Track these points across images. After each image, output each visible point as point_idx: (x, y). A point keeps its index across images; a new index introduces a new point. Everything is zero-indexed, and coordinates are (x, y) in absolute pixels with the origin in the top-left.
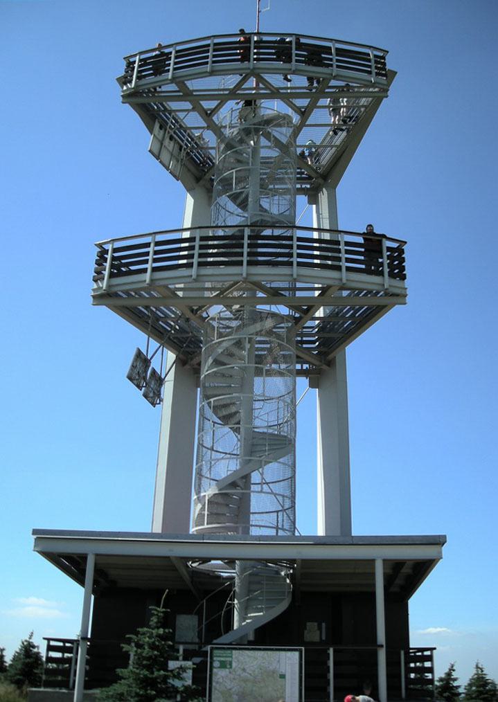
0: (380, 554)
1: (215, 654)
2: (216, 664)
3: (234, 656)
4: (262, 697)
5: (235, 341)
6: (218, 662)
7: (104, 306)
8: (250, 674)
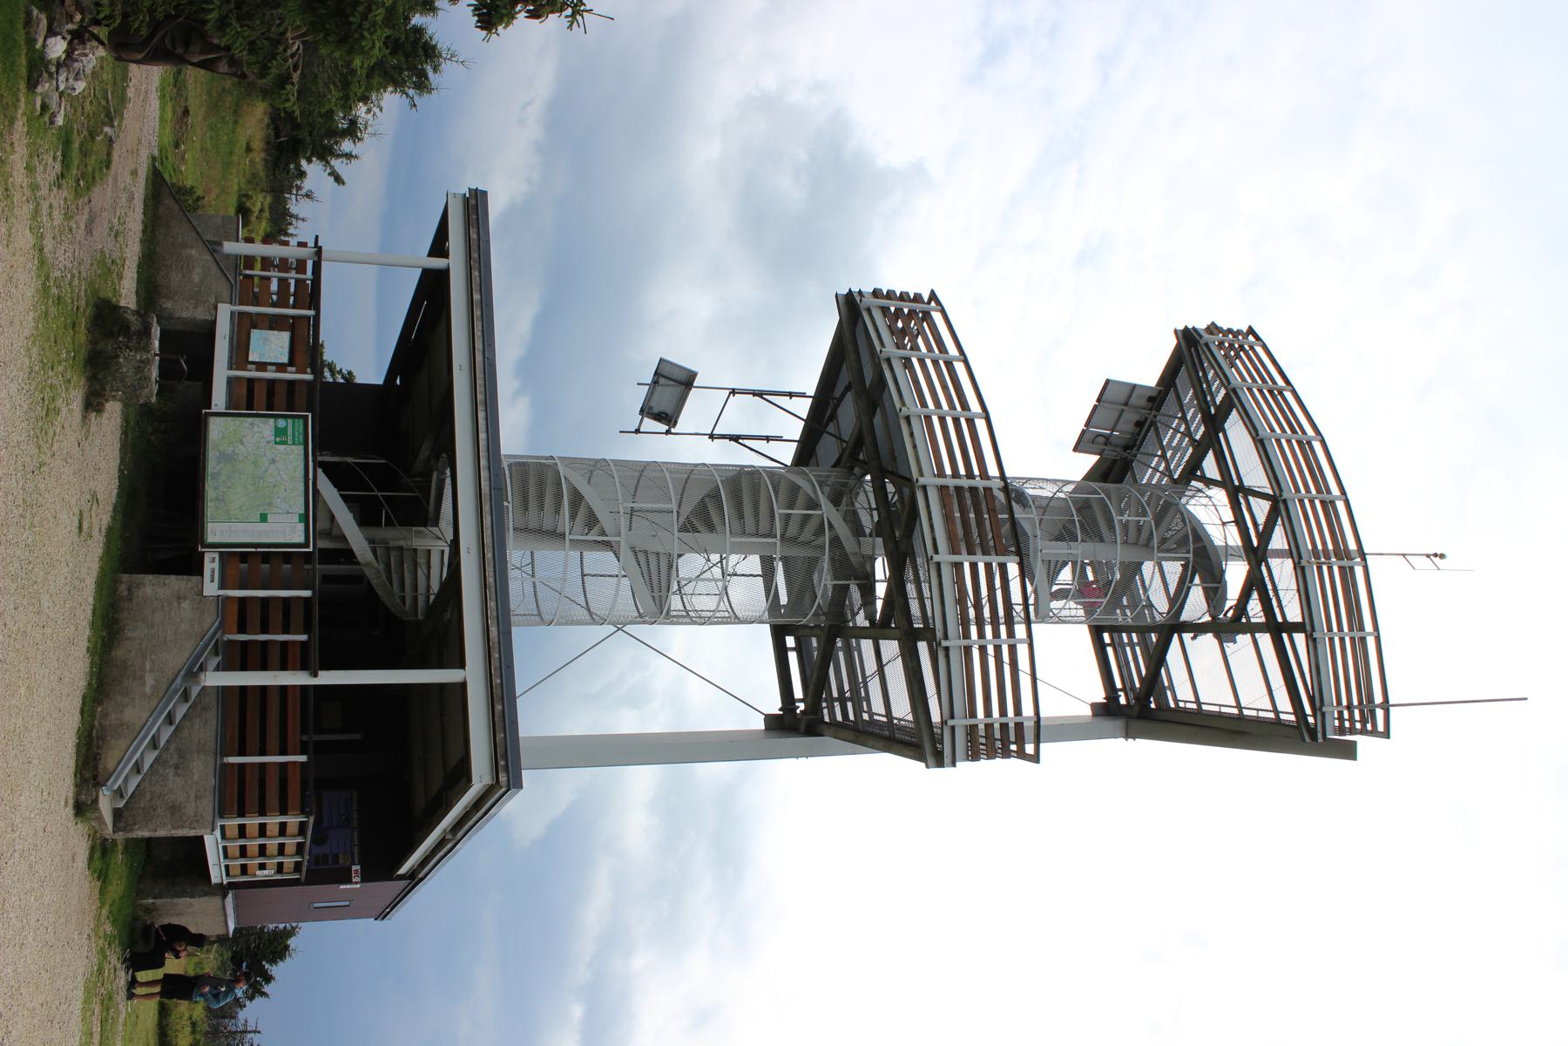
0: (473, 675)
1: (296, 420)
2: (281, 423)
3: (294, 447)
4: (229, 488)
5: (812, 495)
6: (285, 425)
8: (266, 471)
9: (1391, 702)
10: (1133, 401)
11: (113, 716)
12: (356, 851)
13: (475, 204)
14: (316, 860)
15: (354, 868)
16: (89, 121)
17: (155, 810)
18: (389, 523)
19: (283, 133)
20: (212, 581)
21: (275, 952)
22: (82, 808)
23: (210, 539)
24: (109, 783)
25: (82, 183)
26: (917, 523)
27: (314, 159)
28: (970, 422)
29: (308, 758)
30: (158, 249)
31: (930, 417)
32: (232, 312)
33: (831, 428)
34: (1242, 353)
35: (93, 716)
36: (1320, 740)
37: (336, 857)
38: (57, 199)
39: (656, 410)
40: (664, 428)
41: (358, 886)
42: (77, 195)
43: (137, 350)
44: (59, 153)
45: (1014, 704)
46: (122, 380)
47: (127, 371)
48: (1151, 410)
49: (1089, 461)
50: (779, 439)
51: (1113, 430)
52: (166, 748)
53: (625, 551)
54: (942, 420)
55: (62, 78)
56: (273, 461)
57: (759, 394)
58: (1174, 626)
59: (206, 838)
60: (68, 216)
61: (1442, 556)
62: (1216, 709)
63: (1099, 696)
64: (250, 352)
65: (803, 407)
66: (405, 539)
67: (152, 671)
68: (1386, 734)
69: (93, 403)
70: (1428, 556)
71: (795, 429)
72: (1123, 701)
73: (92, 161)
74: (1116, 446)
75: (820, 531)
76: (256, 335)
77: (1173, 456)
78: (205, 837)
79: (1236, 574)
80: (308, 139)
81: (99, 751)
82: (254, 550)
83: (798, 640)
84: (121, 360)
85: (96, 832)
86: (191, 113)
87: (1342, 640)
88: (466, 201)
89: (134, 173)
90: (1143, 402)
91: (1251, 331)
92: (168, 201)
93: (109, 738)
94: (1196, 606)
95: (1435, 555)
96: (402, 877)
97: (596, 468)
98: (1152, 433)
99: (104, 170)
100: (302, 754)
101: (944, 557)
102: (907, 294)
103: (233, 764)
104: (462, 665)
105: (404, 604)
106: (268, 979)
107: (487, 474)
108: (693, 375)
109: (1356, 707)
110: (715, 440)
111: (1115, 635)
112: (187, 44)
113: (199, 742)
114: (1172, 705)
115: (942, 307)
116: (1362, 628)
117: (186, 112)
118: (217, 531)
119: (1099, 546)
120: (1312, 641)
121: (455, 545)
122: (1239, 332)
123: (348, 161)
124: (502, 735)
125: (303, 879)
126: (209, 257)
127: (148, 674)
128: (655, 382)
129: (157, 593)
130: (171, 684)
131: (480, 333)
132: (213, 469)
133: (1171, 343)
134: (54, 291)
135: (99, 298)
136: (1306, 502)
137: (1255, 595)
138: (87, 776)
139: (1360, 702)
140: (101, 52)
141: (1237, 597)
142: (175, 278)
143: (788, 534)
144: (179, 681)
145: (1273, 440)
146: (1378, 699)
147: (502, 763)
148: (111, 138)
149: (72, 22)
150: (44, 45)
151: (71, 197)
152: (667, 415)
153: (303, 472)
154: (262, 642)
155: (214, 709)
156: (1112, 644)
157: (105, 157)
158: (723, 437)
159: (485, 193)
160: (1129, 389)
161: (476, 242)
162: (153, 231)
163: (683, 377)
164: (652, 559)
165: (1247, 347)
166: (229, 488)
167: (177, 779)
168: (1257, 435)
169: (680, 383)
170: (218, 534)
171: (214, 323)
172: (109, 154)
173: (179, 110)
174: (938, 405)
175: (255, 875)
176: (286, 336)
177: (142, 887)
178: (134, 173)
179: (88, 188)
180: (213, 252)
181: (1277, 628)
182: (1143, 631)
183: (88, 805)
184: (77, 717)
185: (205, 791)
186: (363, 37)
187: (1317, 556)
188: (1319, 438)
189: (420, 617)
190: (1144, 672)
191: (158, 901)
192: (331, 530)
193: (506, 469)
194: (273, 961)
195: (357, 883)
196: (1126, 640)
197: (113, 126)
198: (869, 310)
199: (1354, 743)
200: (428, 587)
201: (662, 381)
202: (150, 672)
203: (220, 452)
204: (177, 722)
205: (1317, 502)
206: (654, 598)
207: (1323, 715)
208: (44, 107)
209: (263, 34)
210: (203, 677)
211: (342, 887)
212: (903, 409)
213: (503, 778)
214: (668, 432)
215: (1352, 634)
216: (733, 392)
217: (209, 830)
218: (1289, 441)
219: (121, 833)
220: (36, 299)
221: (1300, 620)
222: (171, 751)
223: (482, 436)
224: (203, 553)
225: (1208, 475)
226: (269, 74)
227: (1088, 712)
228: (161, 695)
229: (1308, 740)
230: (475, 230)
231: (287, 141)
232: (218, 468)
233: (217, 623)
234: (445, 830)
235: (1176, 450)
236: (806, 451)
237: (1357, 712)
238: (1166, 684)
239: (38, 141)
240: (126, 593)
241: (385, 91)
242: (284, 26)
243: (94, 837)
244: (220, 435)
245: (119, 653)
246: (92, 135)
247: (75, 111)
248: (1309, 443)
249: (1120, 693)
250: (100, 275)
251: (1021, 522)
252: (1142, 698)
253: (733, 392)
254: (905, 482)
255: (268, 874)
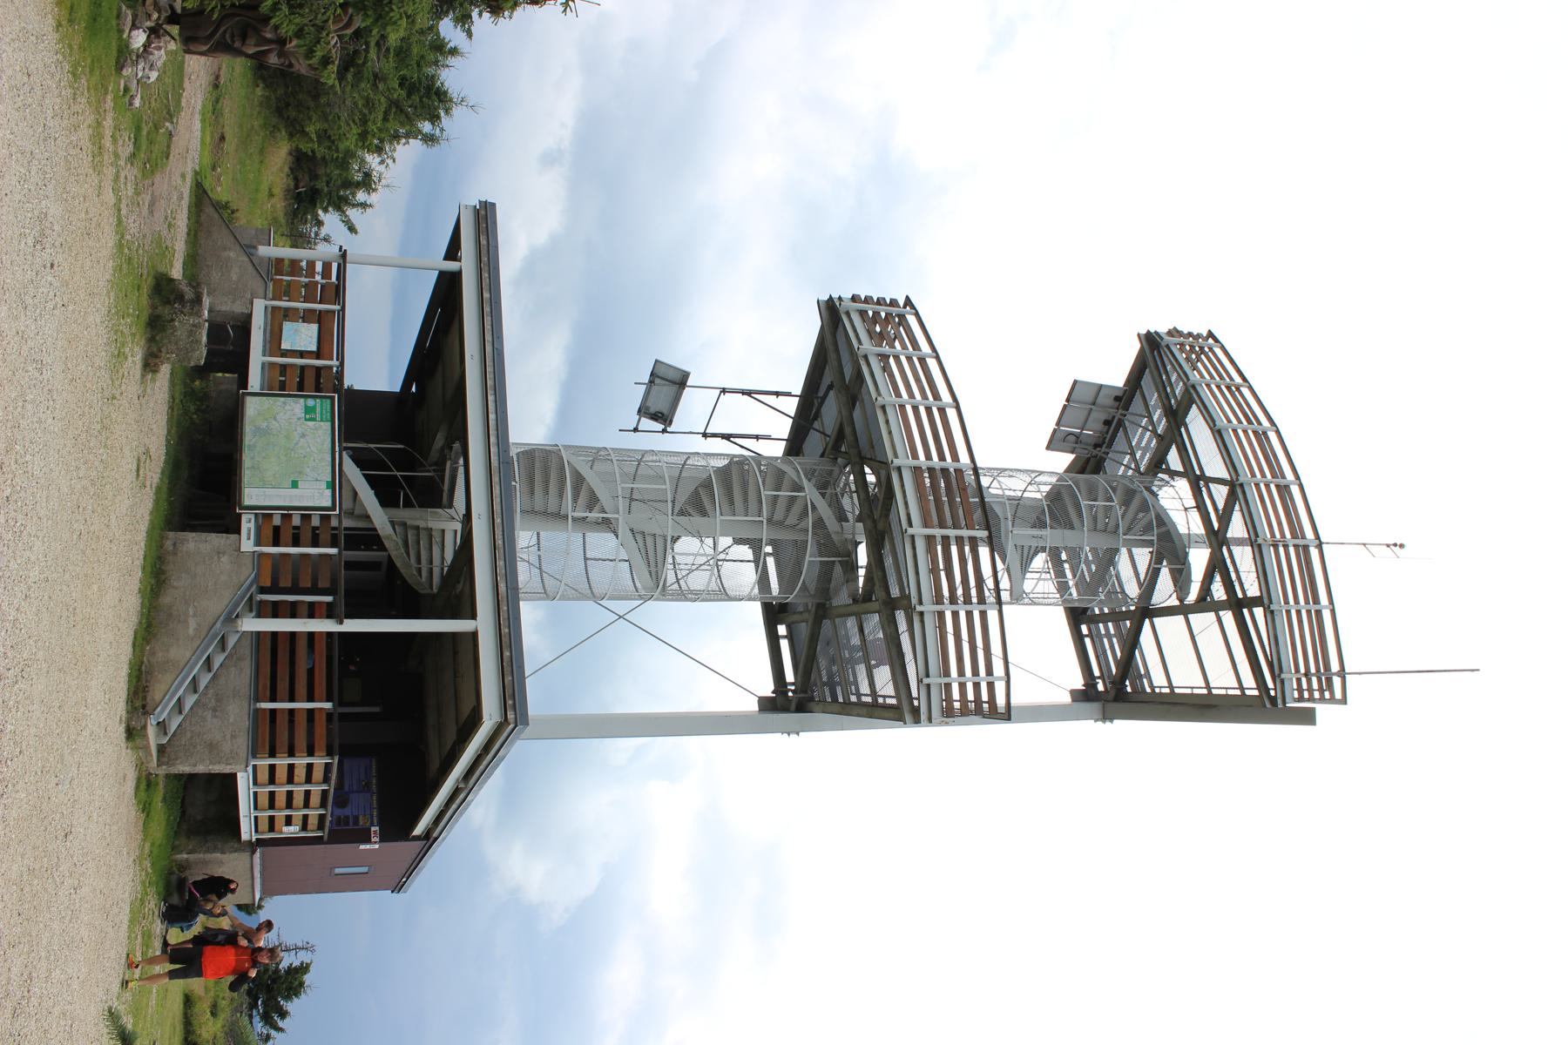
0: (483, 624)
1: (324, 400)
2: (311, 402)
3: (322, 423)
4: (264, 458)
5: (796, 480)
7: (820, 324)
8: (297, 444)
9: (1347, 671)
10: (1099, 401)
11: (160, 654)
12: (375, 813)
13: (485, 216)
14: (338, 821)
15: (373, 829)
16: (154, 115)
17: (195, 747)
18: (408, 504)
19: (301, 184)
20: (249, 539)
21: (291, 988)
22: (133, 734)
23: (247, 502)
24: (156, 712)
25: (148, 166)
26: (894, 503)
27: (330, 209)
28: (942, 411)
29: (334, 706)
30: (200, 251)
31: (904, 406)
32: (266, 307)
33: (816, 425)
34: (1203, 356)
35: (142, 651)
36: (1280, 706)
37: (356, 819)
38: (130, 173)
39: (652, 410)
40: (660, 427)
41: (377, 846)
42: (144, 176)
43: (191, 314)
44: (132, 136)
45: (986, 665)
46: (176, 344)
47: (181, 335)
48: (1118, 409)
49: (1062, 460)
50: (768, 438)
51: (1082, 430)
52: (205, 693)
53: (623, 529)
54: (915, 409)
55: (140, 67)
56: (303, 436)
57: (748, 393)
58: (1146, 611)
59: (239, 775)
60: (137, 193)
61: (1402, 546)
62: (1188, 691)
63: (1078, 683)
64: (283, 342)
65: (791, 406)
66: (421, 519)
67: (195, 615)
68: (1344, 701)
69: (150, 364)
70: (1388, 546)
71: (783, 428)
72: (1101, 687)
73: (156, 148)
74: (1086, 444)
75: (804, 513)
76: (288, 327)
77: (1143, 456)
78: (238, 774)
79: (1199, 559)
80: (326, 189)
81: (148, 684)
82: (286, 512)
83: (789, 628)
84: (176, 324)
85: (142, 763)
86: (227, 139)
87: (1299, 612)
88: (477, 212)
89: (183, 176)
90: (1110, 402)
91: (1211, 335)
92: (209, 210)
93: (156, 673)
94: (1164, 592)
95: (1395, 545)
96: (418, 838)
97: (597, 455)
98: (1121, 434)
99: (165, 160)
100: (328, 701)
101: (918, 530)
102: (884, 299)
103: (265, 709)
104: (473, 616)
105: (420, 575)
106: (283, 1014)
107: (497, 450)
108: (686, 375)
109: (1313, 675)
110: (708, 438)
111: (1092, 626)
112: (244, 38)
113: (235, 688)
114: (1148, 690)
115: (916, 311)
116: (1316, 601)
117: (222, 138)
118: (252, 495)
119: (1068, 532)
120: (1270, 614)
121: (468, 517)
122: (1199, 336)
123: (363, 210)
124: (510, 678)
125: (326, 838)
126: (246, 259)
127: (191, 618)
128: (651, 382)
129: (199, 548)
130: (213, 626)
131: (490, 327)
132: (250, 441)
133: (1132, 349)
134: (126, 251)
135: (157, 271)
136: (1262, 486)
137: (1218, 578)
138: (137, 705)
139: (1318, 670)
140: (172, 46)
141: (1201, 579)
142: (215, 276)
143: (776, 518)
144: (218, 625)
145: (1230, 430)
146: (1335, 667)
147: (510, 702)
148: (171, 132)
149: (150, 20)
150: (129, 36)
151: (139, 176)
152: (663, 414)
153: (330, 445)
154: (292, 602)
155: (249, 659)
156: (1090, 635)
157: (165, 149)
158: (714, 435)
159: (493, 205)
160: (1096, 389)
161: (486, 248)
162: (196, 235)
163: (677, 377)
164: (649, 541)
165: (1206, 349)
166: (264, 458)
167: (215, 720)
168: (1215, 425)
169: (673, 382)
170: (254, 497)
171: (250, 315)
172: (169, 147)
173: (217, 137)
174: (911, 395)
175: (281, 832)
176: (314, 327)
177: (177, 843)
178: (183, 176)
179: (152, 172)
180: (249, 255)
181: (1238, 604)
182: (1116, 617)
183: (137, 730)
184: (129, 649)
185: (240, 732)
186: (392, 10)
187: (1276, 547)
188: (1275, 428)
189: (435, 590)
190: (1119, 654)
191: (192, 857)
192: (353, 509)
193: (515, 458)
194: (288, 998)
195: (375, 842)
196: (1103, 632)
197: (172, 123)
198: (848, 313)
199: (1313, 710)
200: (443, 558)
201: (657, 381)
202: (193, 617)
203: (255, 426)
204: (215, 670)
205: (1273, 487)
206: (650, 572)
207: (1282, 682)
208: (126, 89)
209: (310, 21)
210: (240, 623)
211: (362, 847)
212: (879, 398)
213: (511, 716)
214: (664, 431)
215: (1308, 607)
216: (724, 391)
217: (243, 766)
218: (1245, 432)
219: (164, 767)
220: (115, 251)
221: (1258, 594)
222: (210, 696)
223: (492, 416)
224: (240, 515)
225: (1173, 468)
226: (315, 57)
227: (1067, 699)
228: (202, 637)
229: (1268, 705)
230: (485, 237)
231: (305, 191)
232: (254, 440)
233: (253, 575)
234: (458, 780)
235: (1145, 450)
236: (795, 445)
237: (1314, 680)
238: (1143, 672)
239: (120, 117)
240: (171, 548)
241: (398, 143)
242: (328, 14)
243: (140, 768)
244: (256, 412)
245: (166, 600)
246: (156, 127)
247: (144, 103)
248: (1265, 433)
249: (1098, 681)
250: (157, 254)
251: (994, 506)
252: (1117, 684)
253: (724, 391)
254: (882, 467)
255: (292, 830)
